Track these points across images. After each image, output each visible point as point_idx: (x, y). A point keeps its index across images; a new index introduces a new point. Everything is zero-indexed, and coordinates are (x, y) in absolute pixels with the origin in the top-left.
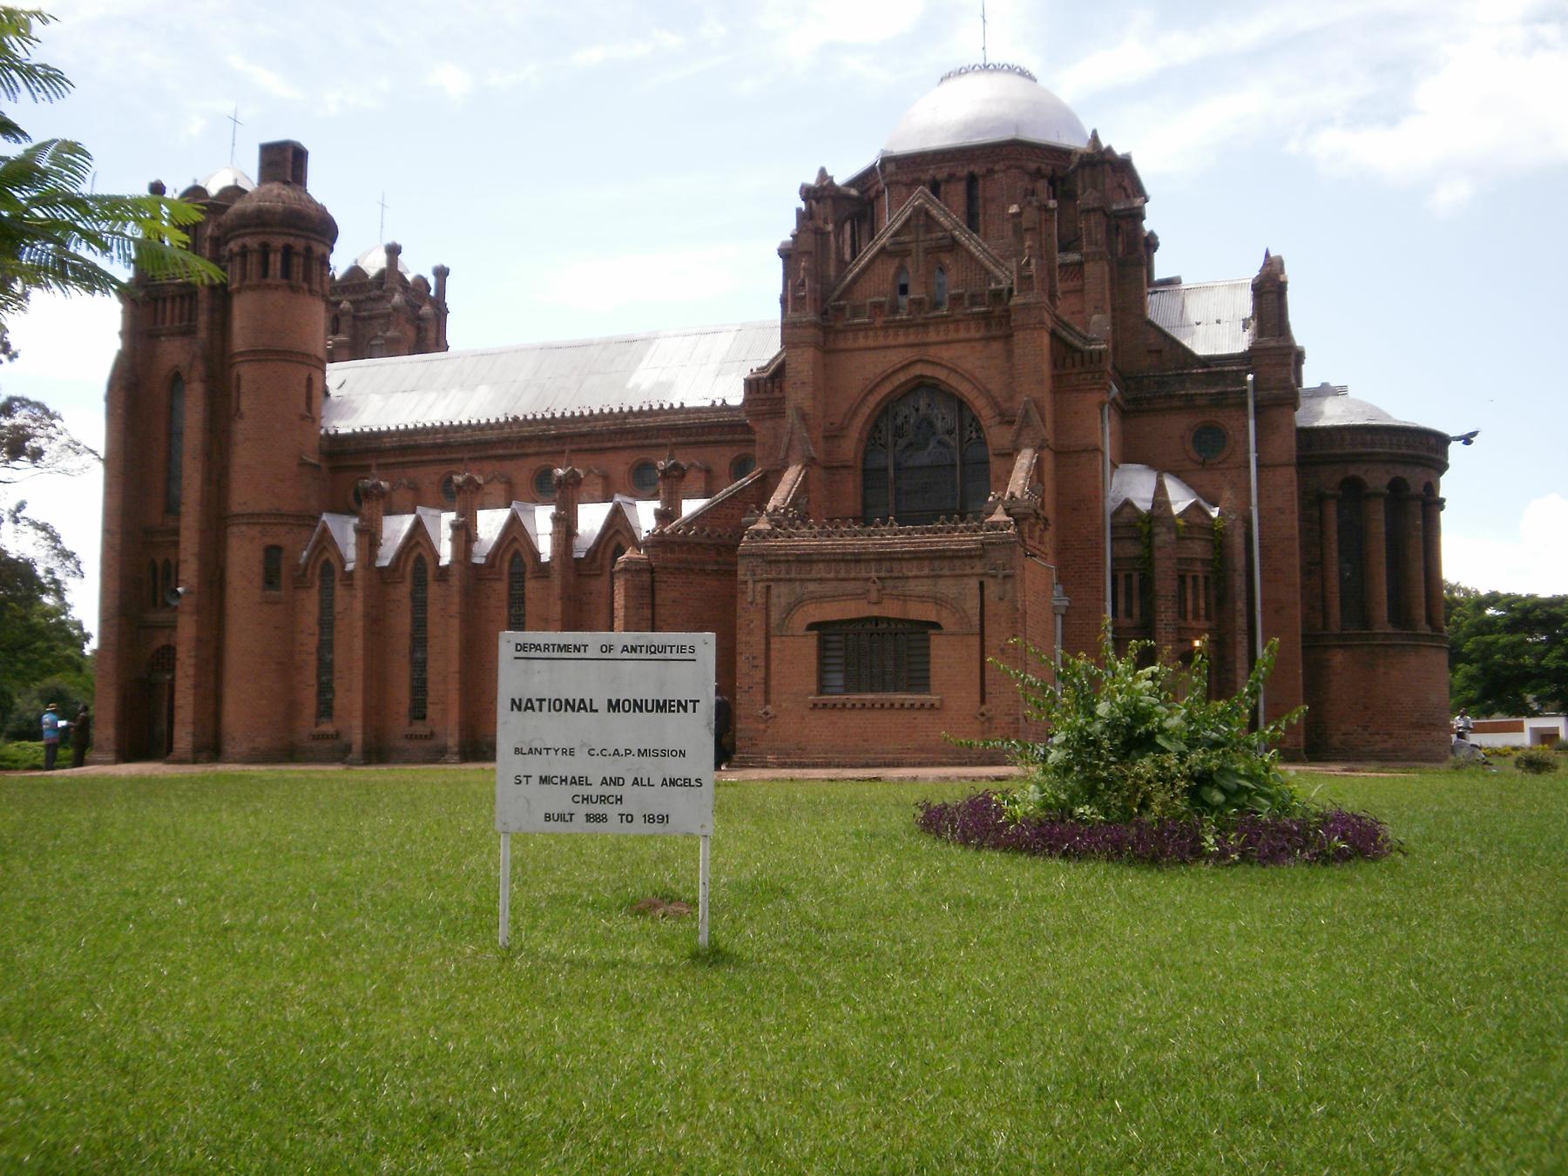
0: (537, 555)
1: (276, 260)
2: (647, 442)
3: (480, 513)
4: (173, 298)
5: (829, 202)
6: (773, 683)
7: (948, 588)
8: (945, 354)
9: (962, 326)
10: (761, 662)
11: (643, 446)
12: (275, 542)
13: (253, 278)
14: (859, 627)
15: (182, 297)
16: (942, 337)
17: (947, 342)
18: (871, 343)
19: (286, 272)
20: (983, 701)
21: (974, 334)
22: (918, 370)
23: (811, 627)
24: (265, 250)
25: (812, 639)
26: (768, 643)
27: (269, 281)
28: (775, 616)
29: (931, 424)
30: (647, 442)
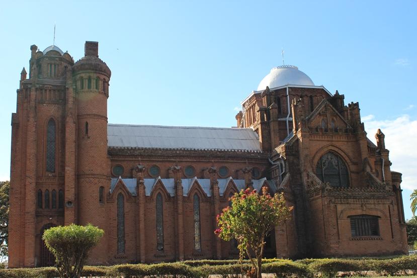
0: (205, 195)
1: (93, 82)
2: (224, 161)
3: (9, 179)
4: (50, 90)
5: (57, 82)
6: (340, 233)
7: (381, 207)
8: (337, 144)
9: (341, 137)
10: (336, 227)
11: (223, 162)
12: (103, 186)
13: (86, 89)
14: (361, 217)
15: (54, 90)
16: (336, 140)
17: (338, 141)
18: (318, 139)
19: (89, 87)
20: (393, 238)
21: (344, 140)
22: (331, 148)
23: (348, 217)
24: (90, 79)
25: (349, 220)
26: (337, 222)
27: (84, 90)
28: (338, 215)
29: (332, 163)
30: (224, 161)
